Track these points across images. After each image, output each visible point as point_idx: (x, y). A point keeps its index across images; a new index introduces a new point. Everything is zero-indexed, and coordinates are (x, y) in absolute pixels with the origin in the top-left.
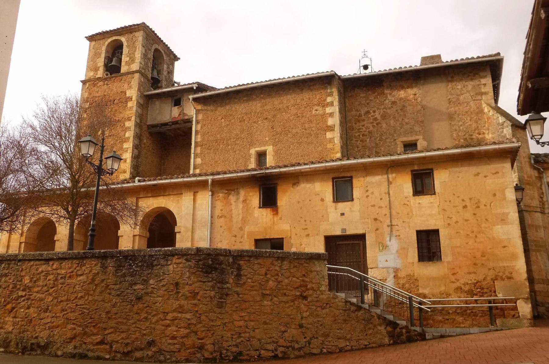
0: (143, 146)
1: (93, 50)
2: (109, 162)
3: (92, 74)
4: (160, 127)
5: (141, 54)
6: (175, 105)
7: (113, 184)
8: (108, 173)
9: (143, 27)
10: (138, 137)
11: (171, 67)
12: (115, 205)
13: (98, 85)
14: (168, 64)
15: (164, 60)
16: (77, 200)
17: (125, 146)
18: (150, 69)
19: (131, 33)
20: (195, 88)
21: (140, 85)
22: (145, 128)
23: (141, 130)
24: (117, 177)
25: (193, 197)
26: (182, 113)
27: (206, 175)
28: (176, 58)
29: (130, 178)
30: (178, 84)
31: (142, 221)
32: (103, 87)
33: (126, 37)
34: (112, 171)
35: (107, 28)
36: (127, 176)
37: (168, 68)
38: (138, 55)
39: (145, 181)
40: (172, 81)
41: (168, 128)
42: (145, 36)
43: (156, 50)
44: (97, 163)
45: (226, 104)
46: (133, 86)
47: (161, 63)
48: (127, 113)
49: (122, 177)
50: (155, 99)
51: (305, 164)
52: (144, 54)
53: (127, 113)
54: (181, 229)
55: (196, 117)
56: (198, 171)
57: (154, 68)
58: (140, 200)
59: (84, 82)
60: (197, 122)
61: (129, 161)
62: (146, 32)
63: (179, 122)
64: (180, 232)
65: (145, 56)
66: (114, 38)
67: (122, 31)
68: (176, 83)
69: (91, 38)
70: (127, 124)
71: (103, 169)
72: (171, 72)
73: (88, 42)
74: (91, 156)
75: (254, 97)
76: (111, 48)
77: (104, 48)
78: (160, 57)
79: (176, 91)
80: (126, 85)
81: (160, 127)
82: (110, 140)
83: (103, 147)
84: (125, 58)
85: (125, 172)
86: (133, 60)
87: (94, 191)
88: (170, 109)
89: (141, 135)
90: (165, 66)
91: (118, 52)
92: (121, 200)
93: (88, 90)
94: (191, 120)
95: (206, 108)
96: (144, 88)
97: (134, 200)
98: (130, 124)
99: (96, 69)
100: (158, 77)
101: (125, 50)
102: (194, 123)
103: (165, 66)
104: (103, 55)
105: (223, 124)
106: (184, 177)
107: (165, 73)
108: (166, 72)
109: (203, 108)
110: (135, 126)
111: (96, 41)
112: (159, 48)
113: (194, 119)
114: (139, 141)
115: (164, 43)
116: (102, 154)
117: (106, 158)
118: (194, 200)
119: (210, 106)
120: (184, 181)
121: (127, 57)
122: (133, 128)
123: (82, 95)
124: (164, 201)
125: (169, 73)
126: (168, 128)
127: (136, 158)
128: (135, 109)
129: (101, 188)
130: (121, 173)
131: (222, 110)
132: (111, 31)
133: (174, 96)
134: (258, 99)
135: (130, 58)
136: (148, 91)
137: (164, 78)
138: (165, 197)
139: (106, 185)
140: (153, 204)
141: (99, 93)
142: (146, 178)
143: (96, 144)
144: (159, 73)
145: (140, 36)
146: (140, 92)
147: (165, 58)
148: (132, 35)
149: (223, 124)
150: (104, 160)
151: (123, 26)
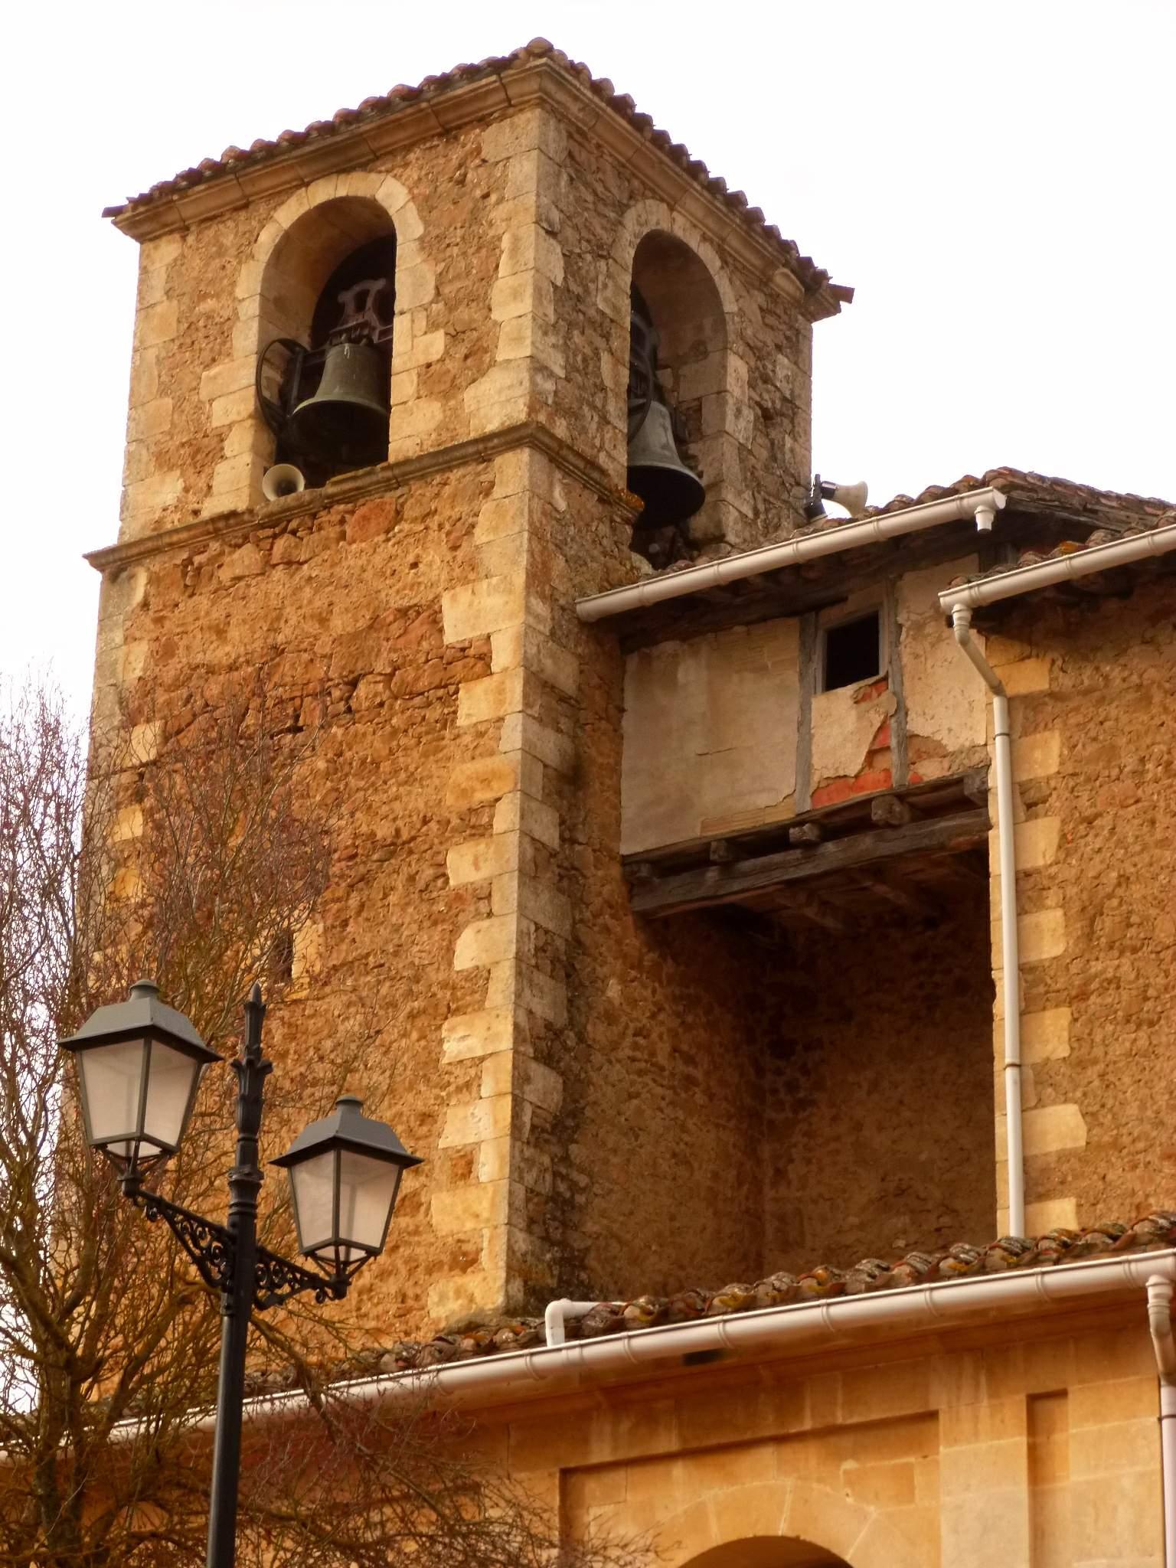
0: (598, 1032)
1: (167, 309)
2: (315, 1188)
3: (168, 490)
4: (727, 867)
5: (538, 293)
6: (834, 680)
7: (372, 1368)
8: (313, 1281)
9: (540, 78)
10: (557, 962)
11: (783, 365)
12: (387, 1541)
13: (225, 575)
14: (757, 353)
16: (89, 1518)
17: (460, 1041)
18: (616, 409)
19: (449, 133)
20: (983, 522)
21: (547, 539)
23: (578, 901)
24: (408, 1305)
25: (1022, 1441)
26: (894, 738)
27: (1123, 1242)
28: (820, 295)
29: (510, 1311)
30: (854, 500)
32: (257, 589)
33: (413, 173)
34: (341, 1265)
36: (487, 1289)
37: (761, 378)
38: (514, 308)
39: (617, 1325)
40: (799, 480)
41: (789, 866)
42: (556, 143)
43: (660, 254)
44: (220, 1209)
46: (491, 559)
47: (700, 351)
48: (460, 777)
49: (445, 1304)
50: (669, 647)
51: (409, 1363)
53: (460, 777)
55: (1014, 762)
56: (1061, 1215)
57: (644, 389)
58: (592, 1486)
59: (113, 565)
60: (1028, 802)
61: (491, 1166)
63: (877, 814)
65: (567, 305)
66: (323, 192)
67: (380, 131)
68: (829, 493)
69: (149, 216)
70: (464, 866)
71: (265, 1256)
72: (784, 414)
73: (129, 248)
74: (167, 1151)
76: (302, 278)
77: (249, 284)
78: (692, 291)
79: (838, 561)
80: (434, 557)
81: (727, 867)
82: (334, 1004)
83: (255, 1069)
84: (413, 343)
85: (464, 1260)
86: (481, 345)
87: (207, 1435)
88: (793, 711)
89: (576, 942)
90: (737, 368)
92: (431, 1501)
93: (147, 620)
94: (971, 788)
96: (576, 563)
97: (539, 1489)
98: (484, 867)
99: (201, 453)
100: (686, 457)
101: (413, 276)
102: (999, 808)
103: (737, 368)
104: (247, 339)
106: (934, 1275)
107: (740, 425)
108: (749, 415)
110: (529, 874)
111: (184, 230)
113: (998, 779)
114: (563, 992)
115: (716, 187)
116: (250, 1128)
117: (290, 1161)
120: (939, 1312)
121: (433, 326)
122: (508, 894)
123: (104, 668)
124: (789, 1482)
125: (767, 417)
126: (789, 866)
127: (550, 1135)
128: (513, 736)
129: (251, 1408)
130: (433, 1268)
132: (294, 141)
133: (818, 607)
135: (454, 337)
136: (609, 584)
137: (732, 467)
139: (302, 1377)
140: (697, 1518)
141: (234, 633)
142: (631, 1297)
143: (202, 1056)
144: (688, 428)
145: (518, 154)
146: (550, 599)
147: (730, 306)
148: (456, 154)
150: (272, 1177)
151: (383, 91)
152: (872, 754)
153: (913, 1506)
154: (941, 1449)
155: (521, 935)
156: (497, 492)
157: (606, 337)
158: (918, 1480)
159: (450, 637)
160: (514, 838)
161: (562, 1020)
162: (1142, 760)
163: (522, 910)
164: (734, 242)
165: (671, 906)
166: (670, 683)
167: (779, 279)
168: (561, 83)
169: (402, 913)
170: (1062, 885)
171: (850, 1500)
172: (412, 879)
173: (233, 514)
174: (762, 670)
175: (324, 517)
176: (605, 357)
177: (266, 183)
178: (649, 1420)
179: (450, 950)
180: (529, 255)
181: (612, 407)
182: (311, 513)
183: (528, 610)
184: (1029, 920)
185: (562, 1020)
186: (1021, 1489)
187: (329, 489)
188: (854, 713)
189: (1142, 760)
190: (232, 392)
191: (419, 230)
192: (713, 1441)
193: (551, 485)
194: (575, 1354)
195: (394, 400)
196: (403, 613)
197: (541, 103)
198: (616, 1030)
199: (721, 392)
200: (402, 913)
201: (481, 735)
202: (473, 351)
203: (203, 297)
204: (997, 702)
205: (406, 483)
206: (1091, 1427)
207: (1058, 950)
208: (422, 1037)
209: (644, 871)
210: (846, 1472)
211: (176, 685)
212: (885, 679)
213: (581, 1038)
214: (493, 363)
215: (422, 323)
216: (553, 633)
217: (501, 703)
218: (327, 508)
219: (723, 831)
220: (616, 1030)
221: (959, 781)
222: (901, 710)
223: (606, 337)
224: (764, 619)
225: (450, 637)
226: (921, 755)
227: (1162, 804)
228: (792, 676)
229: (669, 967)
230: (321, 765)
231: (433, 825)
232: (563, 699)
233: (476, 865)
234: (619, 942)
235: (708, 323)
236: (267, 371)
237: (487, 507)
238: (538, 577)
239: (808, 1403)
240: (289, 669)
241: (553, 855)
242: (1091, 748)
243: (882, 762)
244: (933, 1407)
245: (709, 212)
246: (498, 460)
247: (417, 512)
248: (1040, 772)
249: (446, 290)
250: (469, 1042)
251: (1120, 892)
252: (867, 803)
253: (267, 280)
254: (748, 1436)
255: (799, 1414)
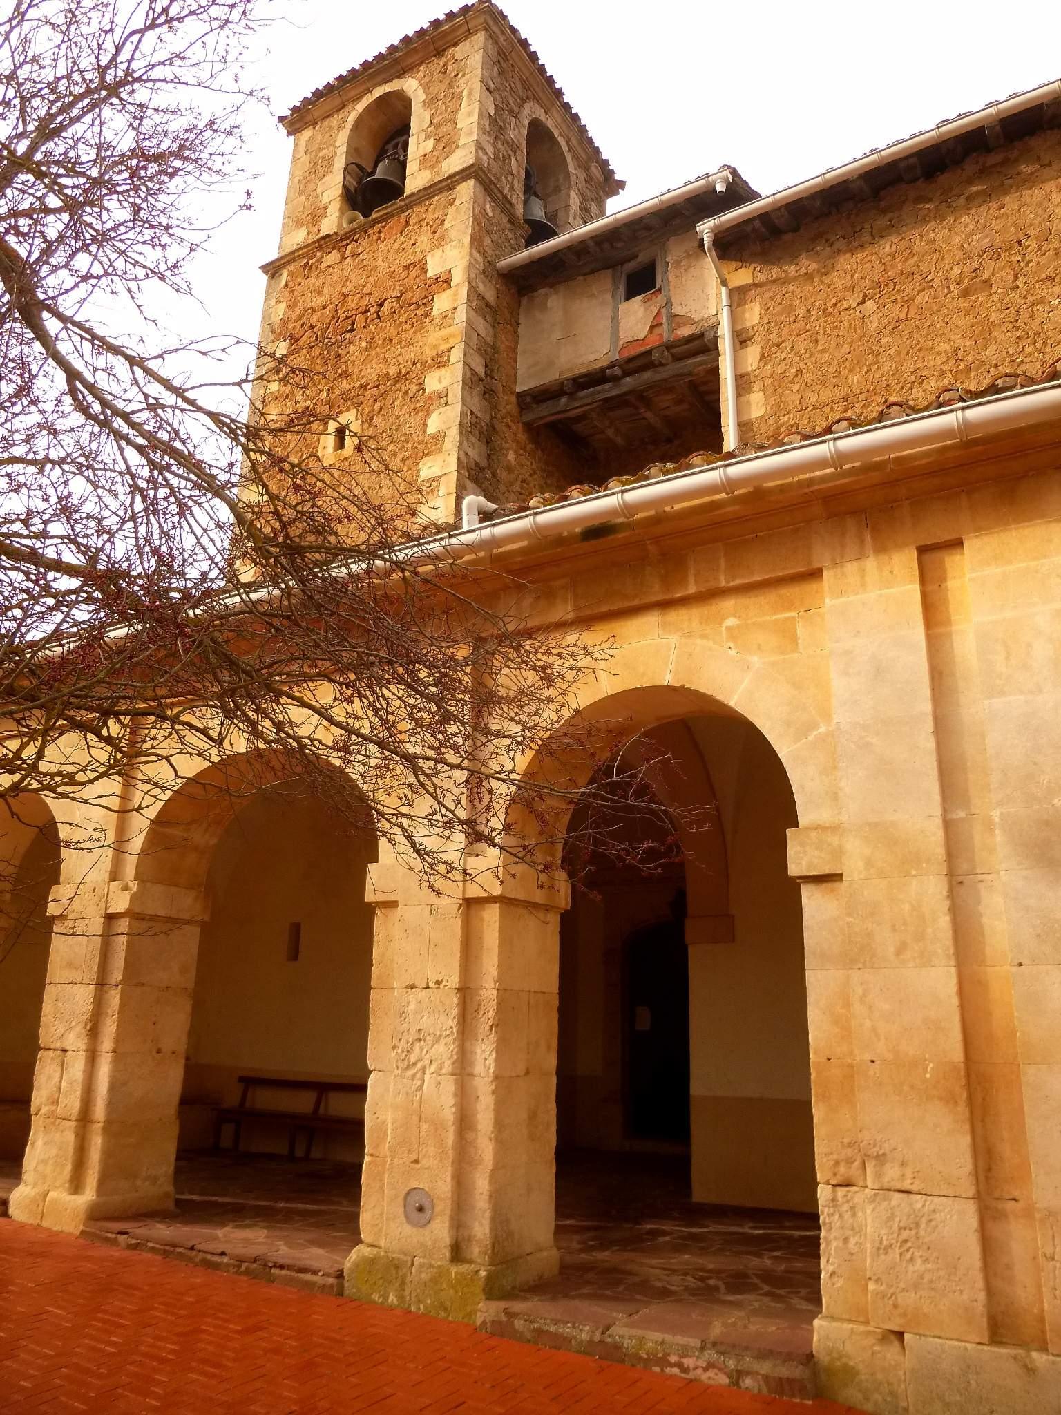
0: (502, 474)
6: (629, 296)
13: (323, 266)
15: (567, 173)
17: (427, 469)
19: (439, 53)
22: (508, 404)
23: (493, 407)
25: (916, 588)
31: (528, 796)
33: (421, 74)
35: (354, 61)
43: (537, 133)
45: (877, 236)
46: (453, 234)
47: (557, 189)
50: (542, 291)
52: (493, 121)
53: (434, 339)
54: (838, 853)
55: (733, 320)
60: (741, 339)
62: (496, 42)
64: (835, 877)
66: (378, 92)
75: (1026, 169)
77: (342, 138)
80: (424, 239)
84: (418, 146)
86: (451, 132)
88: (608, 313)
91: (396, 147)
93: (286, 293)
95: (775, 272)
98: (447, 380)
99: (316, 216)
101: (419, 119)
104: (340, 163)
105: (874, 323)
109: (762, 278)
112: (550, 123)
113: (725, 331)
115: (567, 106)
118: (934, 611)
119: (793, 259)
122: (456, 392)
123: (266, 316)
124: (674, 639)
128: (461, 316)
131: (854, 268)
132: (366, 65)
134: (1047, 172)
135: (438, 140)
138: (677, 616)
141: (326, 291)
145: (472, 55)
146: (484, 254)
147: (571, 169)
149: (874, 323)
152: (652, 327)
153: (795, 655)
154: (827, 601)
155: (463, 414)
156: (457, 202)
157: (515, 152)
158: (802, 632)
159: (430, 274)
160: (461, 365)
161: (484, 463)
162: (809, 311)
163: (463, 400)
164: (574, 141)
165: (541, 418)
166: (544, 307)
167: (593, 169)
168: (495, 19)
169: (402, 409)
170: (762, 380)
171: (733, 652)
172: (406, 392)
173: (328, 236)
174: (593, 296)
175: (371, 231)
176: (513, 161)
177: (353, 93)
178: (548, 595)
179: (425, 424)
180: (477, 95)
181: (516, 183)
182: (364, 230)
183: (471, 255)
184: (743, 399)
185: (484, 463)
186: (918, 633)
187: (374, 216)
188: (642, 309)
189: (809, 311)
190: (332, 188)
191: (423, 97)
192: (604, 609)
193: (485, 202)
194: (486, 533)
195: (408, 172)
196: (407, 267)
197: (486, 30)
198: (513, 476)
199: (567, 206)
200: (402, 409)
201: (444, 317)
202: (446, 144)
203: (321, 149)
204: (724, 290)
205: (411, 207)
206: (994, 571)
207: (761, 413)
208: (409, 469)
209: (528, 399)
210: (728, 628)
211: (299, 318)
212: (660, 290)
213: (494, 475)
214: (457, 147)
215: (423, 136)
216: (484, 272)
217: (455, 300)
218: (373, 226)
219: (570, 375)
220: (513, 476)
221: (702, 335)
222: (669, 303)
223: (515, 152)
224: (592, 272)
225: (430, 274)
226: (680, 325)
227: (822, 331)
228: (609, 297)
229: (539, 453)
230: (364, 344)
231: (418, 365)
232: (488, 305)
233: (440, 381)
234: (515, 434)
235: (561, 177)
236: (348, 177)
237: (451, 210)
238: (476, 241)
239: (692, 572)
240: (352, 303)
241: (481, 380)
242: (778, 308)
243: (657, 331)
244: (816, 565)
245: (564, 120)
246: (458, 187)
247: (417, 219)
248: (748, 324)
249: (435, 121)
250: (434, 469)
251: (797, 379)
252: (649, 352)
253: (350, 137)
254: (636, 602)
255: (683, 582)
